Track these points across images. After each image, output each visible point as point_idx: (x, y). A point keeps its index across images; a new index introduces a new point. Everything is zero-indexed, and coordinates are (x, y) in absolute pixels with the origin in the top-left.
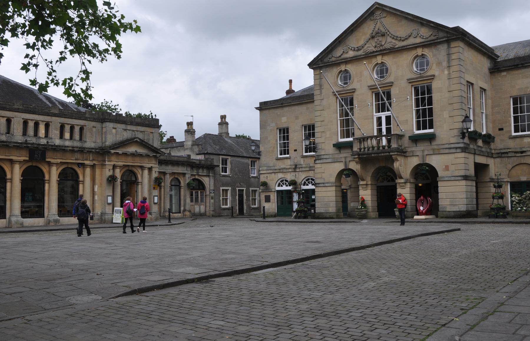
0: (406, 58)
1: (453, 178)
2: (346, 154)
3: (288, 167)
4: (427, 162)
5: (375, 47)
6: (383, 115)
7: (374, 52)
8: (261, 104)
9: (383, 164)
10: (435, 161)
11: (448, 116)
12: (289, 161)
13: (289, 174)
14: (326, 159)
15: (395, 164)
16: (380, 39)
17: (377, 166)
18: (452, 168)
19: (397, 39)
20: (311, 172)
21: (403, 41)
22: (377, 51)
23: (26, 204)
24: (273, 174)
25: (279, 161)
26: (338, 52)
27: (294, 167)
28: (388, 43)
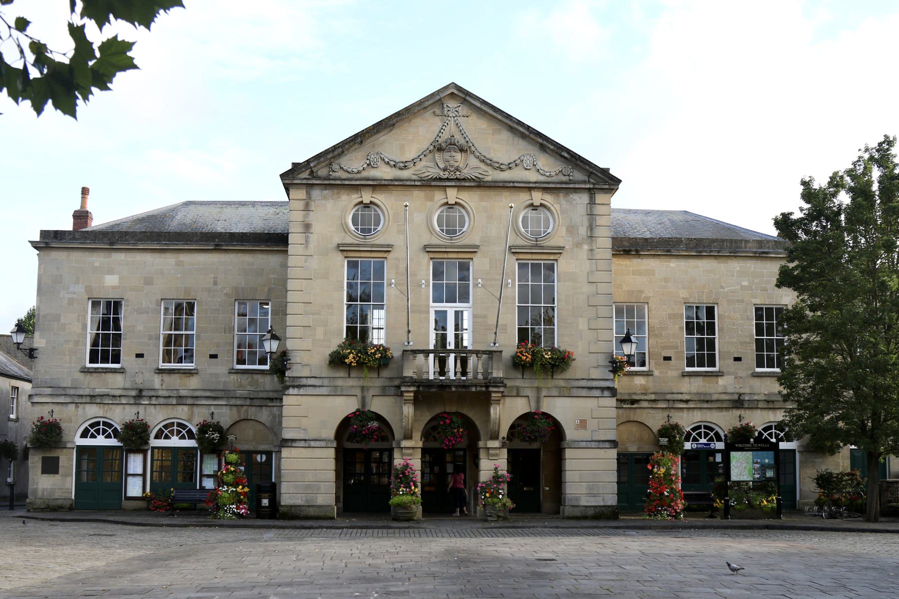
0: (508, 206)
1: (594, 444)
5: (445, 170)
6: (451, 309)
7: (440, 179)
8: (44, 234)
10: (561, 409)
11: (586, 327)
12: (119, 378)
16: (458, 156)
17: (438, 410)
18: (592, 424)
20: (180, 408)
22: (448, 179)
25: (88, 376)
26: (354, 163)
27: (134, 393)
28: (470, 167)
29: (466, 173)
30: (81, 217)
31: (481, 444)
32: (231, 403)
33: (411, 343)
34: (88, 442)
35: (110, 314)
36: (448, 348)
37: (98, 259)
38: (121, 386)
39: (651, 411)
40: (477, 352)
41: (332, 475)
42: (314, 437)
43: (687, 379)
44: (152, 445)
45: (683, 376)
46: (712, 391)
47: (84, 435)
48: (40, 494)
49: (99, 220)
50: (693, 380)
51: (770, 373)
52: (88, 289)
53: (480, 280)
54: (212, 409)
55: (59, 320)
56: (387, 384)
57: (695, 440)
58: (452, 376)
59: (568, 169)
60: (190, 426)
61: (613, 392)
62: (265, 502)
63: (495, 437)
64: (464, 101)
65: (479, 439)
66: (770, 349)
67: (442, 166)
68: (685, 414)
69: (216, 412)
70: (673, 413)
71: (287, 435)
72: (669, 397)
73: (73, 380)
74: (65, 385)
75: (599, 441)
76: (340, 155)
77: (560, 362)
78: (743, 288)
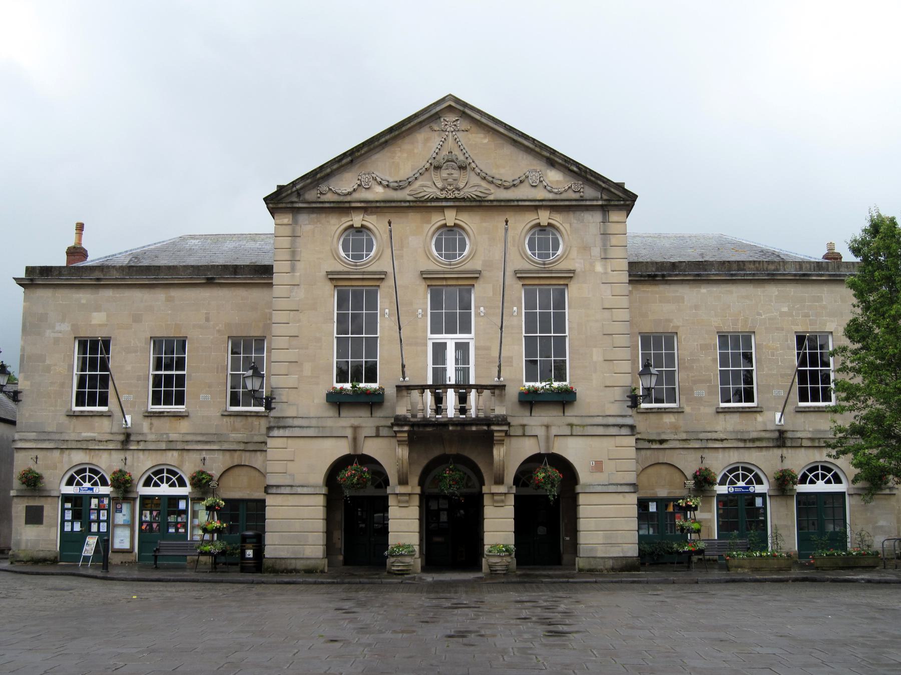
1: (612, 489)
5: (442, 190)
6: (450, 340)
7: (437, 199)
8: (30, 270)
10: (573, 450)
11: (601, 359)
12: (106, 422)
15: (495, 452)
16: (456, 174)
17: (437, 452)
18: (609, 466)
19: (492, 182)
20: (170, 454)
21: (506, 188)
22: (446, 199)
24: (57, 454)
26: (344, 185)
27: (122, 438)
28: (471, 186)
30: (76, 252)
32: (223, 448)
33: (407, 379)
34: (71, 490)
35: (95, 352)
36: (448, 383)
37: (84, 297)
38: (108, 431)
39: (682, 452)
40: (480, 388)
41: (320, 525)
42: (301, 483)
43: (721, 416)
44: (140, 493)
45: (718, 412)
46: (750, 429)
47: (147, 483)
48: (23, 547)
49: (95, 256)
50: (728, 416)
51: (814, 407)
52: (75, 327)
53: (482, 309)
54: (204, 454)
55: (44, 362)
57: (732, 483)
59: (578, 184)
62: (250, 553)
63: (499, 481)
64: (464, 115)
66: (814, 380)
67: (440, 185)
68: (720, 454)
69: (207, 457)
70: (707, 454)
72: (702, 436)
74: (50, 430)
75: (617, 484)
76: (328, 176)
77: (564, 399)
78: (782, 314)
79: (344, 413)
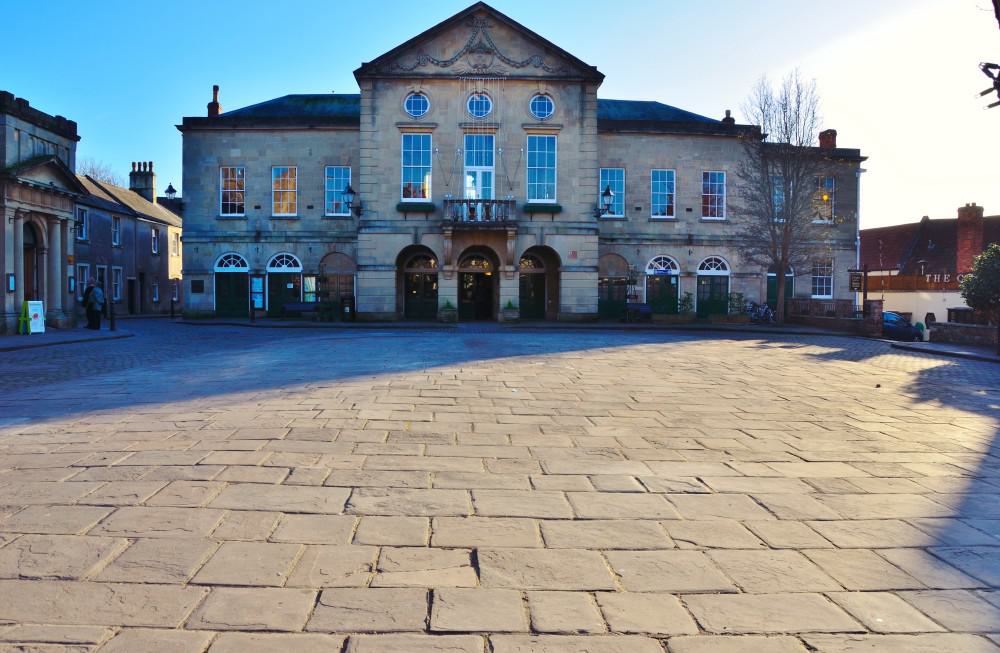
2: (417, 220)
3: (243, 234)
4: (547, 244)
5: (475, 67)
8: (186, 120)
9: (479, 242)
10: (560, 244)
12: (243, 223)
13: (244, 246)
14: (380, 227)
17: (470, 243)
18: (580, 255)
20: (287, 245)
21: (518, 67)
22: (477, 75)
23: (465, 301)
25: (222, 222)
26: (408, 63)
27: (253, 234)
29: (491, 70)
31: (501, 268)
34: (275, 270)
43: (652, 224)
47: (221, 265)
48: (191, 307)
49: (223, 110)
50: (656, 224)
56: (433, 224)
58: (479, 219)
60: (295, 258)
61: (597, 231)
62: (347, 309)
65: (499, 265)
67: (473, 63)
71: (363, 262)
73: (211, 226)
79: (409, 217)
